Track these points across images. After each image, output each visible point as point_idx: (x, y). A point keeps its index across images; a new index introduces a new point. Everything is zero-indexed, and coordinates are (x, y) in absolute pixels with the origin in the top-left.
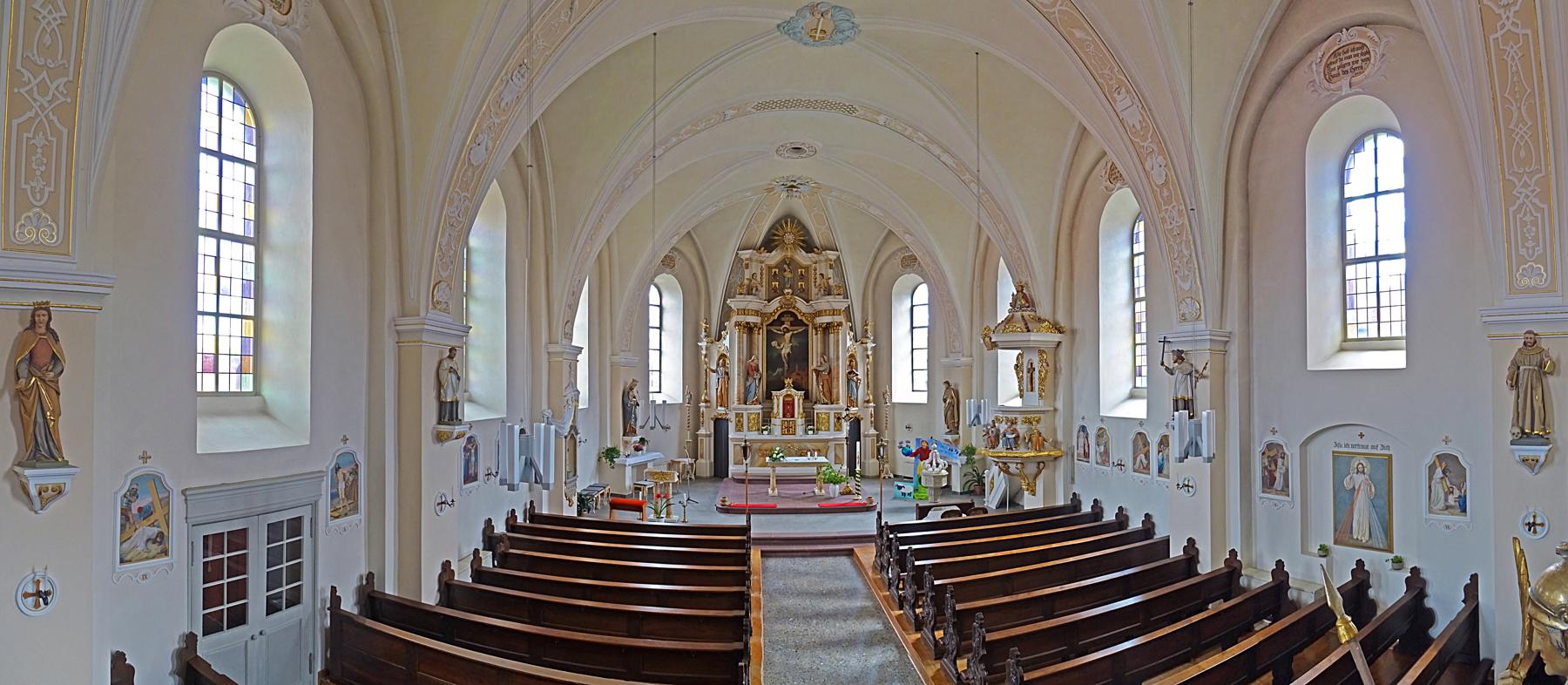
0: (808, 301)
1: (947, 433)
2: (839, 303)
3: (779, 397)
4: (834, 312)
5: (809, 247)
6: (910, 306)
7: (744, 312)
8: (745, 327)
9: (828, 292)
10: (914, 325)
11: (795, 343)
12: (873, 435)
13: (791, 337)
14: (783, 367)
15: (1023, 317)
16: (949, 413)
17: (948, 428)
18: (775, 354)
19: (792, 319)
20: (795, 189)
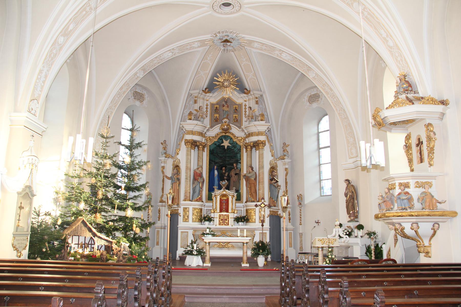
0: (240, 127)
1: (348, 222)
2: (260, 126)
3: (218, 193)
4: (259, 134)
5: (243, 90)
6: (316, 132)
7: (192, 133)
8: (192, 144)
9: (252, 118)
10: (321, 146)
15: (407, 98)
16: (350, 204)
17: (350, 217)
20: (229, 44)
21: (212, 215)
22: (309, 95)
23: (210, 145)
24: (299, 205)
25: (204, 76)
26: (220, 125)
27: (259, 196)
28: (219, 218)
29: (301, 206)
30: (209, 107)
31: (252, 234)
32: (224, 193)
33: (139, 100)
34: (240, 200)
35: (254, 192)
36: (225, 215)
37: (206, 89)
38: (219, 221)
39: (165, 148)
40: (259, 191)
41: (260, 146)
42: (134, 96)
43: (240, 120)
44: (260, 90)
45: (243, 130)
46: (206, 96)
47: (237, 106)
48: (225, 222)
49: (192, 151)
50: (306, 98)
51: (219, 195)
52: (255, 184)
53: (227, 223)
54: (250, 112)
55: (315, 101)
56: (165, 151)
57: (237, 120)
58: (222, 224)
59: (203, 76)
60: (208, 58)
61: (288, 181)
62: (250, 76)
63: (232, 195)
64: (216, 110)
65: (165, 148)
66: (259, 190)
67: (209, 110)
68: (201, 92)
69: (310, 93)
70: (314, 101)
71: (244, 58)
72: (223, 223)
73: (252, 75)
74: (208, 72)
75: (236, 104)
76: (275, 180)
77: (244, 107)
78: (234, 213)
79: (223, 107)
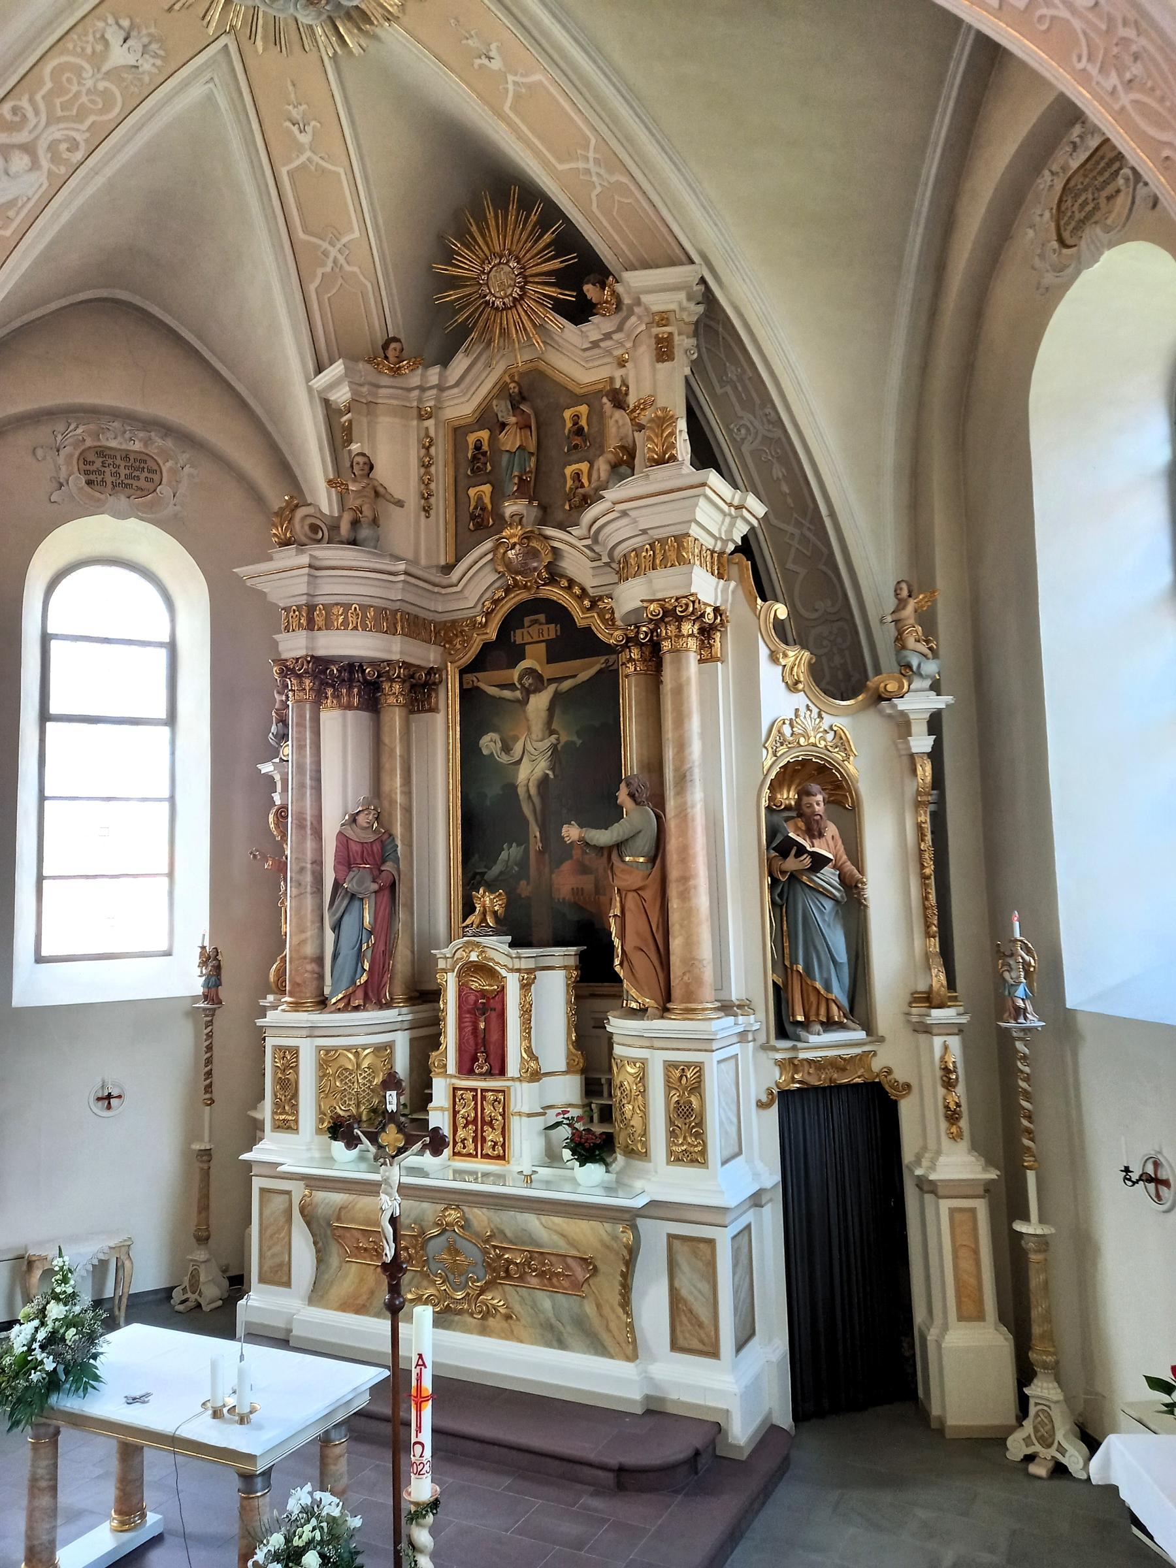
12: (959, 1189)
14: (522, 839)
26: (488, 545)
33: (127, 485)
41: (668, 638)
42: (87, 473)
44: (684, 258)
47: (583, 409)
48: (484, 1140)
55: (1097, 208)
64: (474, 457)
72: (475, 1140)
74: (357, 234)
75: (578, 399)
76: (801, 850)
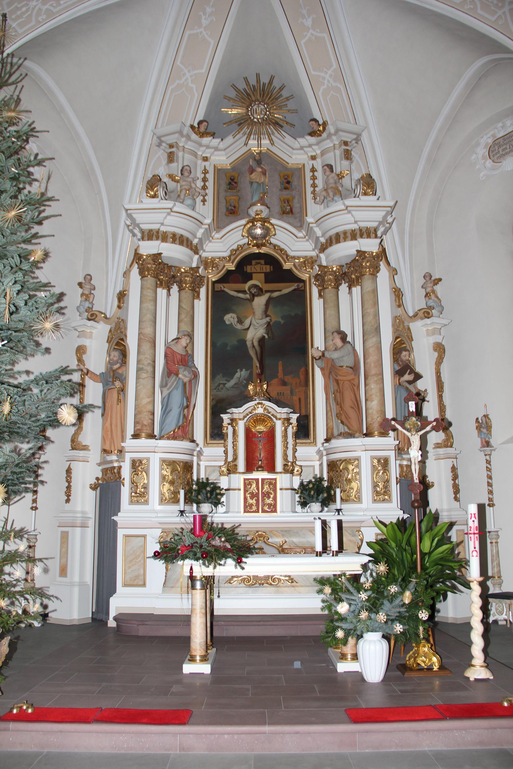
11: (276, 317)
13: (267, 305)
18: (233, 341)
19: (268, 268)
21: (224, 483)
22: (490, 141)
23: (214, 280)
24: (483, 446)
25: (194, 86)
27: (369, 419)
28: (245, 491)
29: (491, 450)
30: (210, 176)
31: (353, 538)
32: (260, 410)
34: (306, 435)
35: (352, 407)
36: (263, 480)
37: (200, 123)
38: (245, 499)
39: (86, 297)
40: (368, 403)
43: (301, 208)
45: (310, 232)
46: (201, 145)
49: (162, 292)
50: (482, 151)
51: (245, 417)
52: (356, 383)
53: (270, 505)
54: (330, 177)
56: (87, 304)
57: (291, 211)
58: (254, 508)
59: (190, 84)
60: (203, 17)
61: (445, 378)
62: (326, 82)
63: (284, 416)
65: (86, 297)
66: (366, 400)
67: (210, 184)
68: (187, 130)
69: (493, 135)
70: (507, 154)
71: (309, 17)
73: (331, 76)
77: (308, 174)
78: (292, 472)
79: (251, 174)
